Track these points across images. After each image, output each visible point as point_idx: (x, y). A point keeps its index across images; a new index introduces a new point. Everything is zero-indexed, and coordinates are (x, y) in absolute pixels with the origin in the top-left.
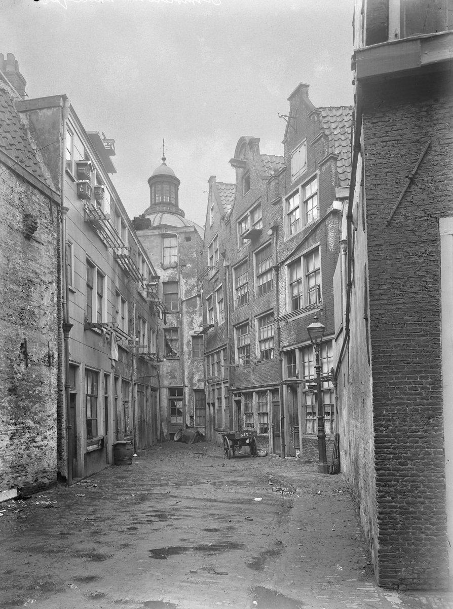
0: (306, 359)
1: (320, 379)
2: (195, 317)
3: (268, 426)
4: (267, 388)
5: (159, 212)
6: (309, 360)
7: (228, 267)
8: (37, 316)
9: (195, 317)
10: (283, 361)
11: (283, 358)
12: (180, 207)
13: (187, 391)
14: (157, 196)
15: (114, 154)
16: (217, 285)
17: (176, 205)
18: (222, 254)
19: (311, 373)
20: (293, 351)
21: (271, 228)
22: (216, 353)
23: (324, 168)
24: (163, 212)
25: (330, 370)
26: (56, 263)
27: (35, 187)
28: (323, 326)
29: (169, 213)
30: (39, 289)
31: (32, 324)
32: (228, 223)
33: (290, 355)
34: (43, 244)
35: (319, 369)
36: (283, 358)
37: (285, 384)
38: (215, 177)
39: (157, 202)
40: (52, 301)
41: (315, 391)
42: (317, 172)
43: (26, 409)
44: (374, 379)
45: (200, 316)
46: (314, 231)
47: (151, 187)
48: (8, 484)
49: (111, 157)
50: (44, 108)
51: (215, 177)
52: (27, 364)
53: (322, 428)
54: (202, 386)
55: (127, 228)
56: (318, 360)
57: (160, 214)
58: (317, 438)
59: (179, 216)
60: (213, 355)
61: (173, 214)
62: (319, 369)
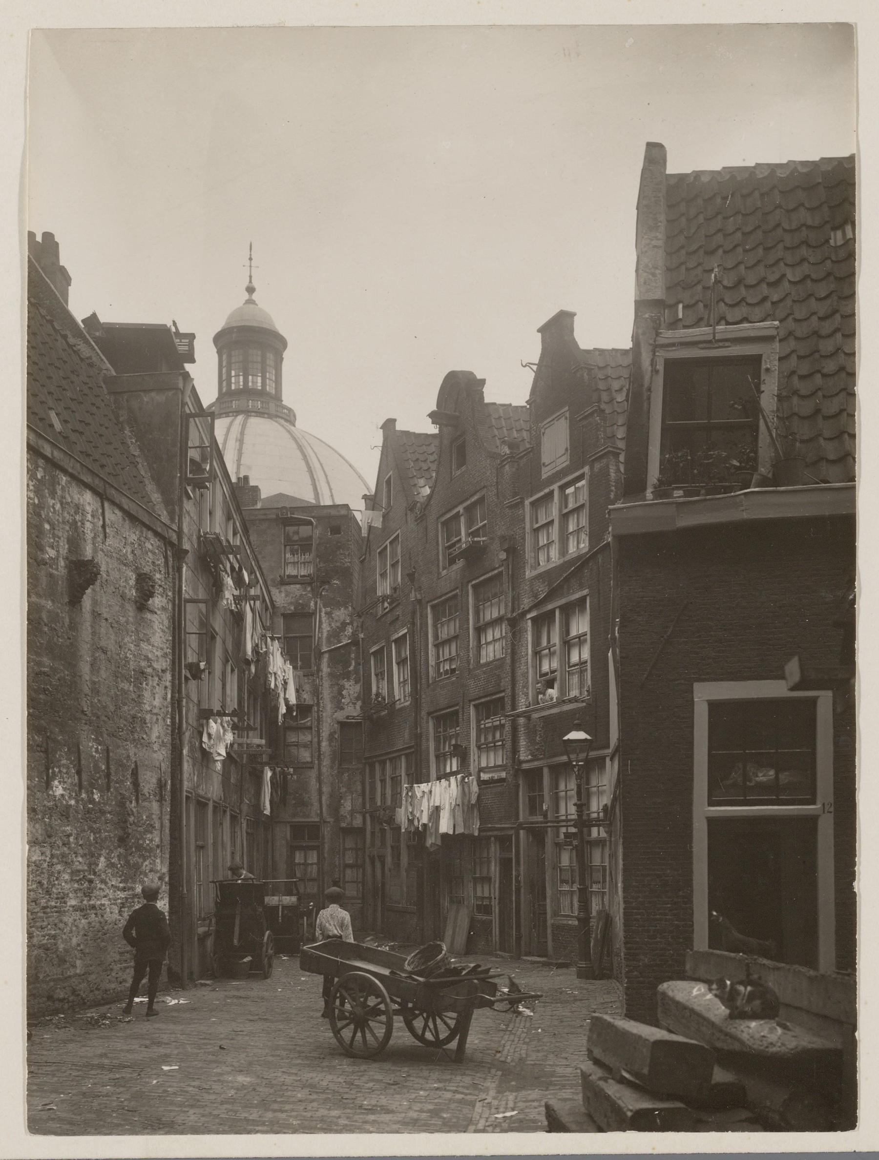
0: (562, 787)
1: (584, 822)
2: (347, 684)
3: (490, 902)
4: (490, 833)
5: (237, 412)
6: (566, 787)
7: (419, 601)
8: (149, 725)
9: (347, 684)
10: (521, 787)
11: (521, 782)
12: (287, 399)
13: (326, 831)
14: (233, 373)
15: (192, 360)
16: (396, 631)
17: (278, 397)
18: (408, 575)
19: (569, 810)
20: (540, 770)
21: (505, 550)
22: (391, 760)
23: (597, 466)
24: (248, 413)
25: (601, 808)
26: (171, 638)
27: (149, 528)
28: (589, 737)
29: (260, 414)
30: (151, 683)
31: (143, 738)
32: (421, 519)
33: (533, 777)
34: (156, 613)
35: (582, 806)
36: (521, 782)
37: (524, 828)
38: (394, 421)
39: (233, 387)
40: (165, 699)
41: (575, 843)
42: (586, 469)
43: (137, 867)
44: (624, 848)
45: (356, 682)
46: (579, 569)
47: (220, 353)
48: (117, 978)
49: (188, 367)
50: (152, 390)
51: (394, 421)
52: (137, 800)
53: (585, 905)
54: (358, 822)
55: (239, 535)
56: (579, 793)
57: (240, 418)
58: (576, 923)
59: (282, 421)
60: (384, 763)
61: (270, 416)
62: (582, 806)
